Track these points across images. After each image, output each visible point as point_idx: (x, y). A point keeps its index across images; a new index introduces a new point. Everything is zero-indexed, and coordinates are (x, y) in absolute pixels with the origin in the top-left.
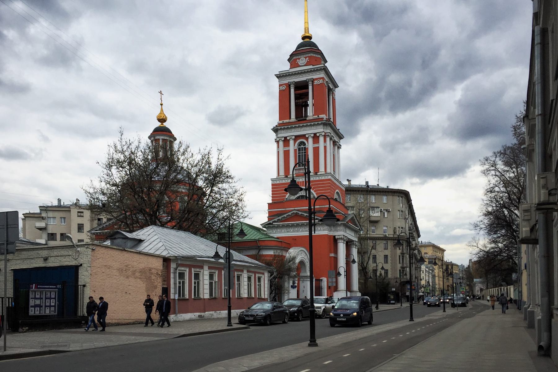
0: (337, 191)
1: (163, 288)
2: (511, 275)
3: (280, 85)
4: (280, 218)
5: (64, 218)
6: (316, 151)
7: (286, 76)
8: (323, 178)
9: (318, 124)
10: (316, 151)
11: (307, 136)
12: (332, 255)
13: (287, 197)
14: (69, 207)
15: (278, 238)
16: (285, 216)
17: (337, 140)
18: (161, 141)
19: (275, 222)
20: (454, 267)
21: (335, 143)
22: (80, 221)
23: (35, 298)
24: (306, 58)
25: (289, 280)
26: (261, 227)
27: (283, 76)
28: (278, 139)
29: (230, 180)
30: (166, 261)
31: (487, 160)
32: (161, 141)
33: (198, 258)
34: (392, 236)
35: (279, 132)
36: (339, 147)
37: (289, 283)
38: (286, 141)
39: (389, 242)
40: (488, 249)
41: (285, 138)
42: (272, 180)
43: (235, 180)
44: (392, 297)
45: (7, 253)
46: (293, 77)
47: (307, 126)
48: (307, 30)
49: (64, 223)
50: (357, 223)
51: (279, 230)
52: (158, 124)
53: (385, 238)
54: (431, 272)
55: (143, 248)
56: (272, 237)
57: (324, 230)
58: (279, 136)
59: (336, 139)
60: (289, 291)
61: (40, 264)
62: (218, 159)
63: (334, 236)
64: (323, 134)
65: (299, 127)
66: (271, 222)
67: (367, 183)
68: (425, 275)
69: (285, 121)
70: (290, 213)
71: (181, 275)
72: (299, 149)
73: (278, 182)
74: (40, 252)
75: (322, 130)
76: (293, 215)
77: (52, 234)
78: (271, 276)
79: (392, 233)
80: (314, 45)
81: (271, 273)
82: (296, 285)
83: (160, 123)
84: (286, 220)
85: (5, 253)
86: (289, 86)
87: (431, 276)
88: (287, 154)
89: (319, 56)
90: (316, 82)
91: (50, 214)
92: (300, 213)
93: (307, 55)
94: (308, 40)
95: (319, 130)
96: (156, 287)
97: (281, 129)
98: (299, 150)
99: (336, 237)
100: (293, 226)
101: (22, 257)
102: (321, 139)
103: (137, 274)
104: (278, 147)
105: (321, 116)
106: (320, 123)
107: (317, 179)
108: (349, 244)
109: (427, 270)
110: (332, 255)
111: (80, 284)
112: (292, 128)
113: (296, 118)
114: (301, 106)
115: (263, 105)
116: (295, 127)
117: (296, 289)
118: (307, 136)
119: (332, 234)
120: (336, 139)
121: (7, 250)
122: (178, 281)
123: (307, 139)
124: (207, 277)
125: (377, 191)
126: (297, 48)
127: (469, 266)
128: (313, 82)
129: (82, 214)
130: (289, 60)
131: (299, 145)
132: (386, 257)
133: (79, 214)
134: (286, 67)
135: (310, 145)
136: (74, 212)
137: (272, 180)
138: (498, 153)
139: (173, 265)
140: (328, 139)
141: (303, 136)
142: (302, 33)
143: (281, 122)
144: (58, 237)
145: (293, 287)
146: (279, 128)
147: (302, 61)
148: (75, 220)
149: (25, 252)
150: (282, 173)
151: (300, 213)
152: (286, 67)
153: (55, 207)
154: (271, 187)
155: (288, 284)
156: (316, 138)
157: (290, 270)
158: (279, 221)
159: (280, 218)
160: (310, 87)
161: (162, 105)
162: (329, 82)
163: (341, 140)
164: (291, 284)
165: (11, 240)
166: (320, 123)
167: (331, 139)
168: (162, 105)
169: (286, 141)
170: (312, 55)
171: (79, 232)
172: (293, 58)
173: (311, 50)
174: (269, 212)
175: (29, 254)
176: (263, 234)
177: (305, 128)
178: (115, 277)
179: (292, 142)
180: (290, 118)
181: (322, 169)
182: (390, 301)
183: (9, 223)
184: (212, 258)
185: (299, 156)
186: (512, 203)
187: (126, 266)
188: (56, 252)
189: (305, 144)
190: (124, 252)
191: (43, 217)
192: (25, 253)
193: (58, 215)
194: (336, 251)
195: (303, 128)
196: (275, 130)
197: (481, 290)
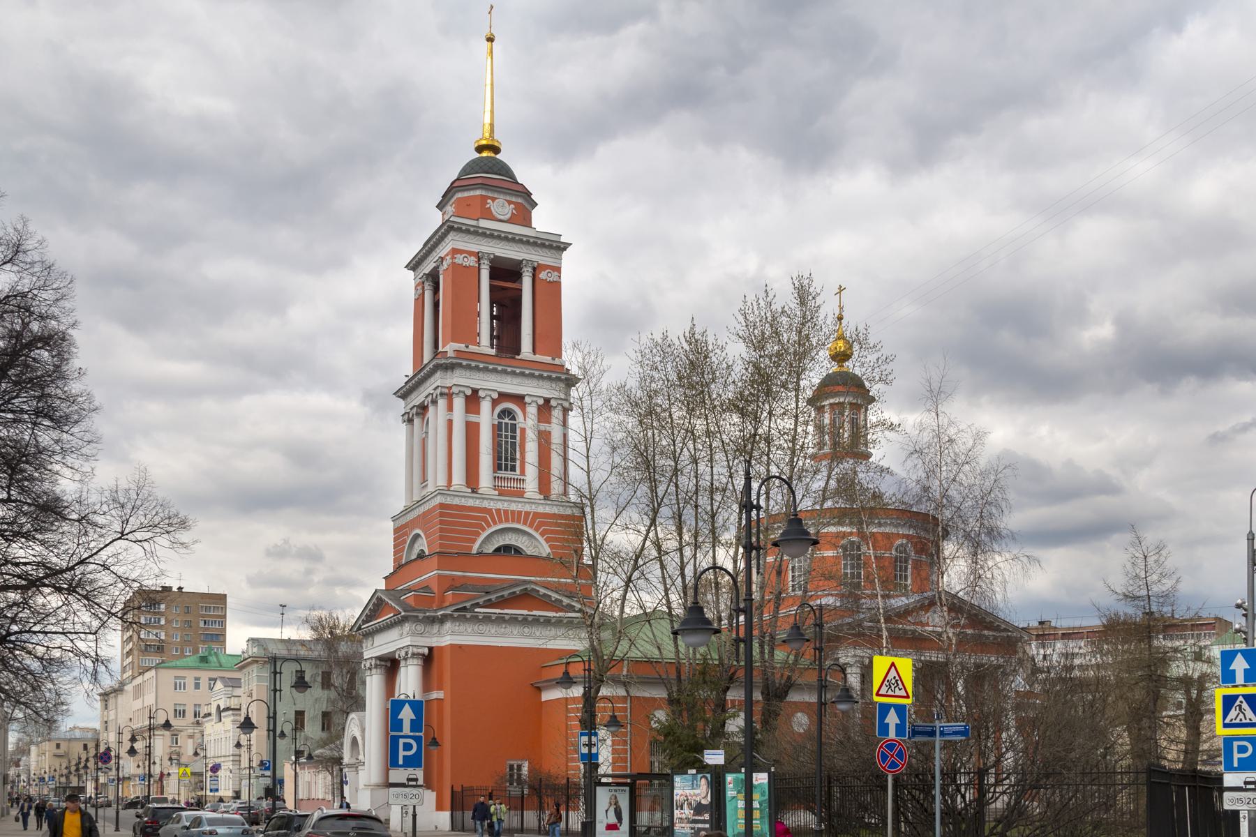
41: (475, 391)
52: (835, 368)
66: (468, 605)
80: (505, 170)
84: (502, 603)
92: (543, 591)
93: (514, 199)
102: (557, 414)
107: (477, 503)
118: (527, 399)
131: (499, 416)
135: (528, 421)
140: (459, 403)
141: (519, 399)
158: (489, 604)
159: (493, 597)
173: (480, 181)
179: (485, 406)
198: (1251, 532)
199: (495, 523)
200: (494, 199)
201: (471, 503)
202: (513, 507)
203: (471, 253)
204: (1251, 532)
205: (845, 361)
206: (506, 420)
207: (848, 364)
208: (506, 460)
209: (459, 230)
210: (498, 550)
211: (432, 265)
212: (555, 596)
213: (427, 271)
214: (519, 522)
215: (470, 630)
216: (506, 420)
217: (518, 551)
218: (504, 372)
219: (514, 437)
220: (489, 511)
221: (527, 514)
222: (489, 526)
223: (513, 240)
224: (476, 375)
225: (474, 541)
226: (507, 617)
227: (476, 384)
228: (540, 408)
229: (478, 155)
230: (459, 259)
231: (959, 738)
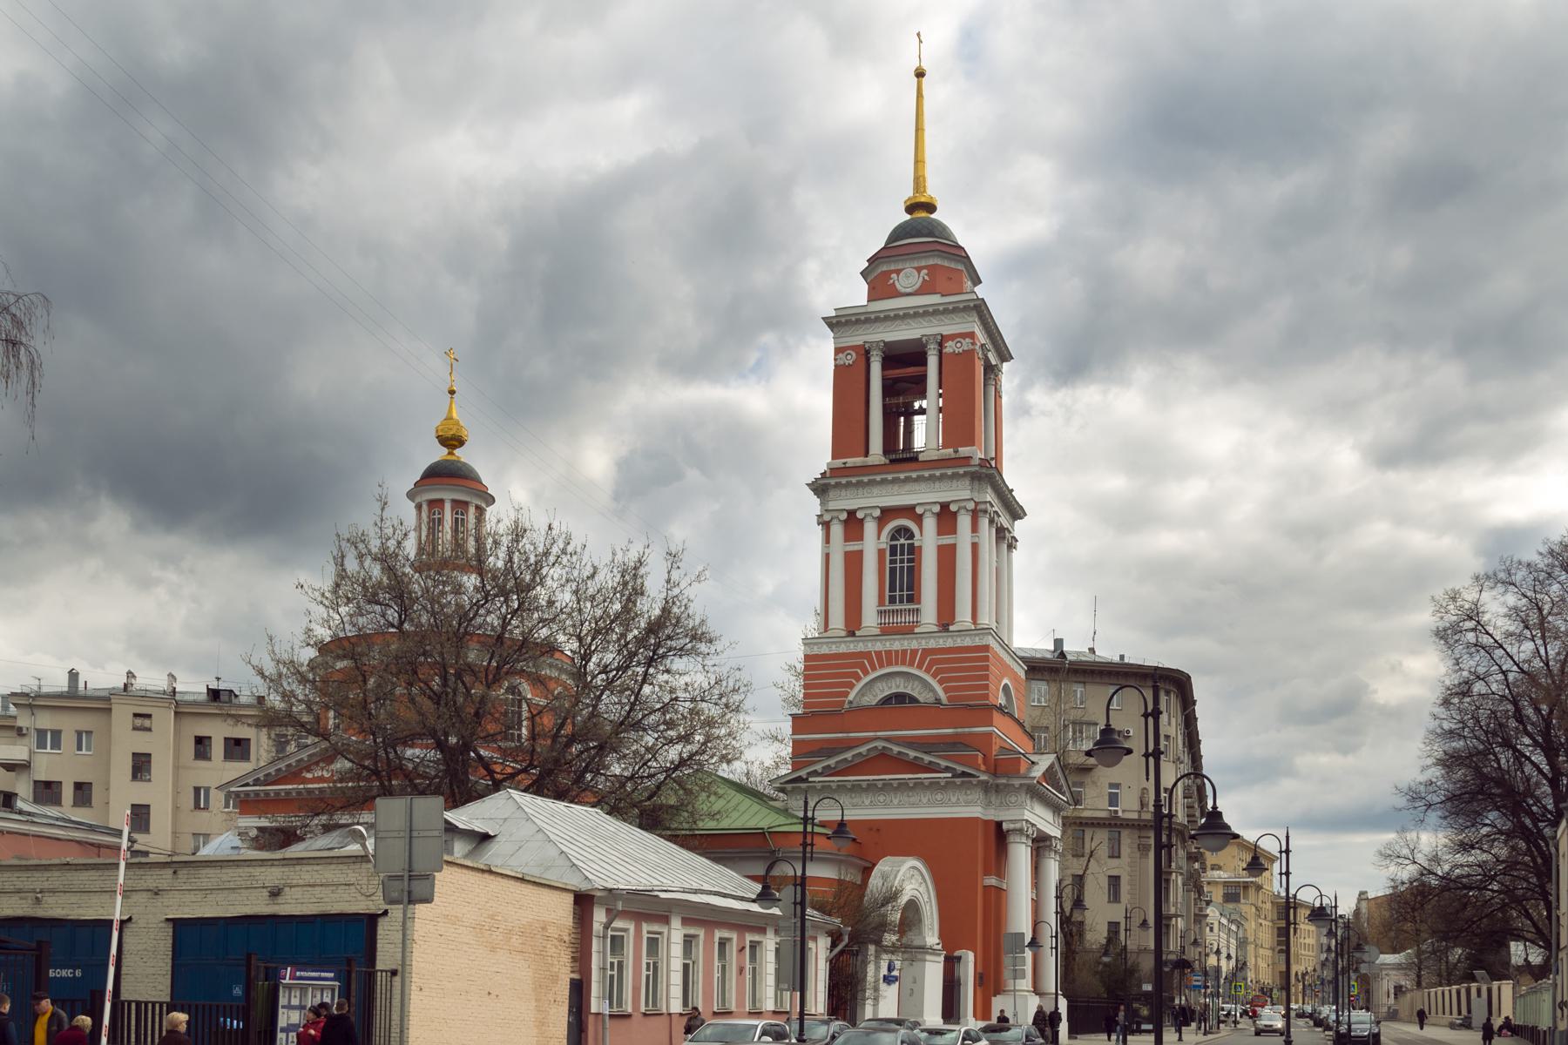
0: (1006, 681)
1: (572, 980)
2: (1508, 947)
3: (838, 351)
4: (832, 762)
5: (89, 733)
6: (947, 556)
7: (858, 322)
8: (968, 642)
9: (955, 476)
10: (947, 556)
11: (919, 510)
13: (851, 697)
14: (108, 699)
16: (848, 755)
17: (1006, 525)
18: (448, 507)
19: (815, 773)
21: (1001, 533)
22: (141, 743)
23: (289, 1007)
24: (919, 269)
25: (877, 957)
26: (769, 791)
27: (848, 323)
28: (827, 518)
29: (703, 647)
30: (583, 902)
31: (1454, 599)
32: (448, 507)
33: (663, 895)
34: (1135, 816)
35: (832, 494)
37: (878, 968)
38: (853, 524)
39: (1125, 833)
40: (1447, 867)
41: (852, 513)
43: (718, 646)
44: (1145, 1012)
45: (410, 902)
46: (880, 327)
47: (919, 479)
49: (88, 749)
50: (1062, 781)
52: (440, 453)
53: (1113, 824)
54: (1234, 927)
55: (493, 855)
57: (968, 803)
58: (832, 505)
59: (1004, 520)
60: (876, 989)
61: (258, 905)
62: (668, 581)
63: (999, 824)
64: (971, 506)
65: (895, 481)
66: (803, 773)
67: (1058, 643)
68: (1228, 939)
69: (851, 461)
70: (863, 749)
71: (617, 943)
72: (893, 550)
73: (825, 650)
74: (257, 871)
75: (966, 494)
76: (873, 754)
77: (48, 784)
78: (834, 945)
79: (1137, 806)
80: (938, 231)
81: (836, 938)
82: (896, 973)
83: (445, 451)
85: (406, 900)
86: (865, 353)
87: (1233, 941)
88: (854, 563)
89: (960, 267)
90: (950, 347)
91: (45, 721)
92: (896, 749)
94: (924, 214)
95: (958, 493)
96: (555, 979)
97: (838, 485)
99: (1005, 826)
100: (871, 788)
101: (205, 883)
102: (964, 522)
103: (516, 941)
104: (827, 540)
105: (964, 451)
106: (961, 471)
107: (949, 643)
109: (1224, 921)
111: (379, 966)
112: (872, 483)
113: (886, 452)
116: (884, 481)
117: (895, 986)
118: (919, 510)
119: (993, 815)
120: (1004, 520)
121: (410, 892)
122: (645, 960)
123: (919, 519)
124: (677, 950)
125: (1092, 672)
126: (888, 243)
127: (1357, 912)
128: (941, 345)
129: (147, 723)
130: (864, 274)
131: (893, 538)
132: (1114, 881)
133: (139, 722)
134: (857, 294)
135: (928, 539)
136: (122, 715)
137: (807, 642)
138: (1488, 578)
139: (599, 916)
141: (909, 511)
142: (908, 192)
143: (839, 463)
144: (68, 793)
145: (888, 980)
146: (833, 482)
147: (909, 278)
148: (126, 742)
149: (208, 871)
150: (838, 620)
151: (896, 749)
152: (857, 294)
153: (60, 696)
155: (875, 970)
156: (947, 518)
157: (883, 926)
159: (832, 762)
160: (932, 362)
162: (989, 346)
163: (1017, 523)
164: (884, 971)
165: (419, 867)
166: (961, 471)
167: (991, 521)
169: (853, 524)
170: (939, 261)
171: (135, 777)
172: (878, 274)
174: (794, 742)
175: (225, 878)
176: (778, 811)
177: (916, 486)
178: (465, 948)
179: (870, 528)
180: (867, 454)
182: (1139, 1024)
183: (1283, 956)
184: (754, 901)
185: (893, 571)
186: (1525, 729)
187: (492, 917)
188: (307, 874)
189: (912, 536)
190: (486, 875)
191: (20, 729)
192: (210, 871)
193: (69, 725)
195: (908, 487)
196: (820, 488)
197: (1399, 990)
199: (874, 669)
200: (898, 272)
202: (914, 645)
205: (455, 447)
206: (902, 541)
207: (456, 452)
210: (887, 700)
212: (912, 754)
214: (903, 663)
215: (925, 800)
217: (913, 700)
218: (908, 480)
219: (892, 562)
220: (867, 655)
221: (914, 652)
222: (866, 673)
223: (916, 315)
224: (944, 485)
225: (852, 686)
226: (849, 785)
228: (939, 516)
229: (908, 217)
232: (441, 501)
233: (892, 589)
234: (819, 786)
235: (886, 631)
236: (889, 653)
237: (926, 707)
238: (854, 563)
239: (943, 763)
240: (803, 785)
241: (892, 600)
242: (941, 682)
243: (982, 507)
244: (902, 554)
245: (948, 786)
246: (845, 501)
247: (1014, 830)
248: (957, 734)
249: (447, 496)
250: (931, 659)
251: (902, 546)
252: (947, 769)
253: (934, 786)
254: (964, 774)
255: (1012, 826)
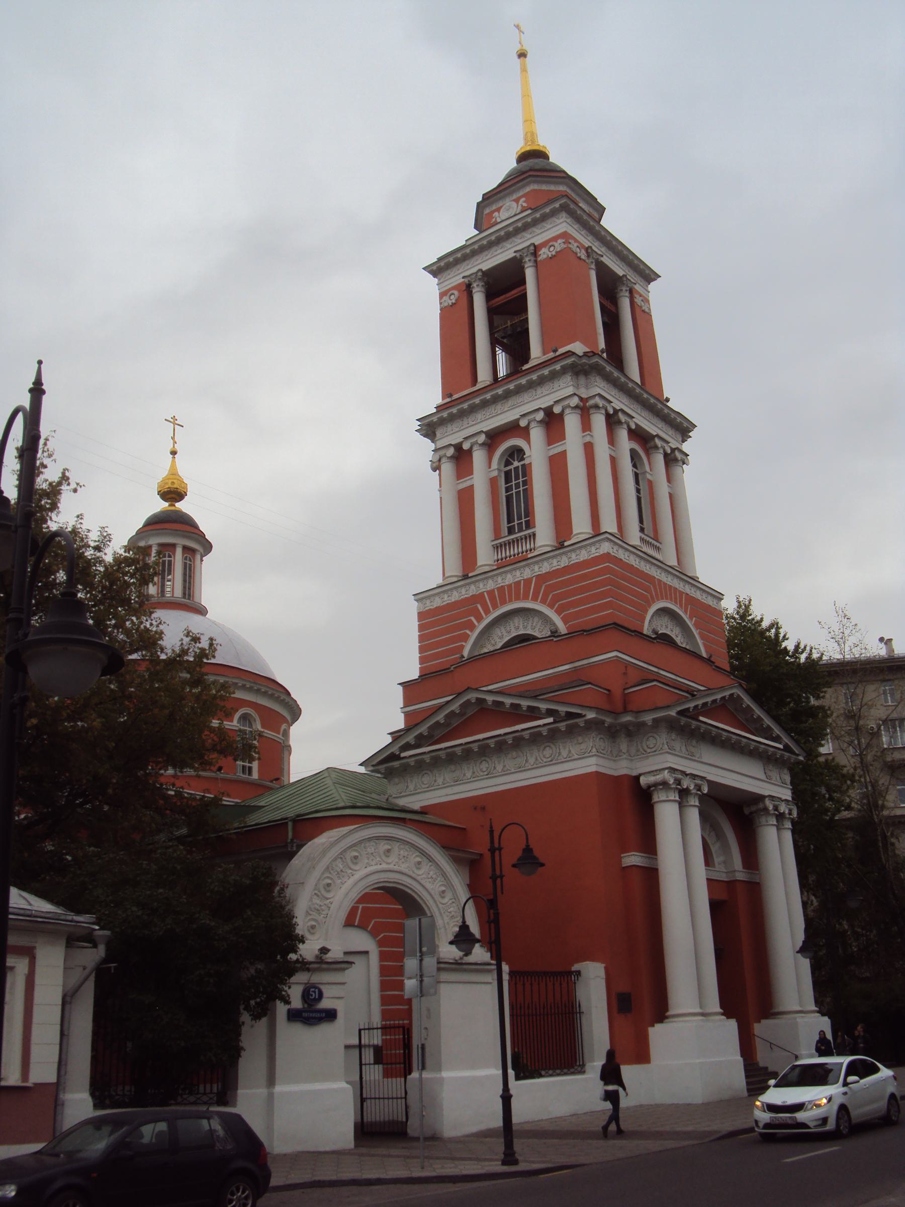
3: (442, 295)
6: (558, 467)
10: (558, 467)
11: (523, 423)
12: (633, 859)
15: (424, 811)
18: (179, 551)
20: (446, 575)
24: (517, 201)
32: (179, 551)
36: (673, 459)
41: (548, 411)
42: (420, 597)
48: (530, 136)
51: (426, 779)
52: (161, 505)
56: (403, 810)
72: (508, 475)
75: (570, 391)
83: (166, 504)
92: (508, 701)
93: (521, 193)
98: (508, 479)
99: (643, 781)
102: (572, 422)
108: (733, 814)
110: (633, 859)
114: (513, 341)
115: (398, 367)
118: (523, 423)
119: (622, 768)
128: (535, 254)
131: (508, 463)
135: (536, 450)
140: (599, 421)
141: (513, 429)
142: (519, 146)
151: (508, 701)
154: (415, 624)
156: (552, 422)
161: (174, 453)
162: (598, 248)
168: (174, 453)
169: (461, 457)
170: (535, 187)
179: (479, 457)
180: (475, 380)
181: (581, 525)
185: (509, 499)
194: (648, 841)
195: (510, 402)
196: (429, 428)
198: (528, 846)
201: (564, 562)
202: (527, 573)
203: (583, 246)
204: (528, 846)
206: (516, 464)
208: (519, 518)
209: (572, 214)
211: (620, 273)
213: (485, 266)
214: (518, 598)
216: (516, 464)
220: (479, 598)
221: (528, 582)
222: (480, 619)
225: (466, 638)
227: (545, 402)
230: (574, 246)
231: (505, 968)
232: (173, 546)
233: (510, 519)
234: (412, 762)
235: (502, 565)
236: (501, 589)
237: (545, 641)
238: (465, 500)
239: (543, 706)
240: (396, 764)
241: (511, 531)
242: (558, 612)
243: (591, 402)
244: (517, 478)
245: (553, 736)
246: (454, 435)
247: (656, 785)
248: (576, 670)
249: (180, 542)
250: (549, 586)
251: (516, 468)
252: (550, 713)
253: (535, 739)
254: (570, 715)
255: (652, 779)
